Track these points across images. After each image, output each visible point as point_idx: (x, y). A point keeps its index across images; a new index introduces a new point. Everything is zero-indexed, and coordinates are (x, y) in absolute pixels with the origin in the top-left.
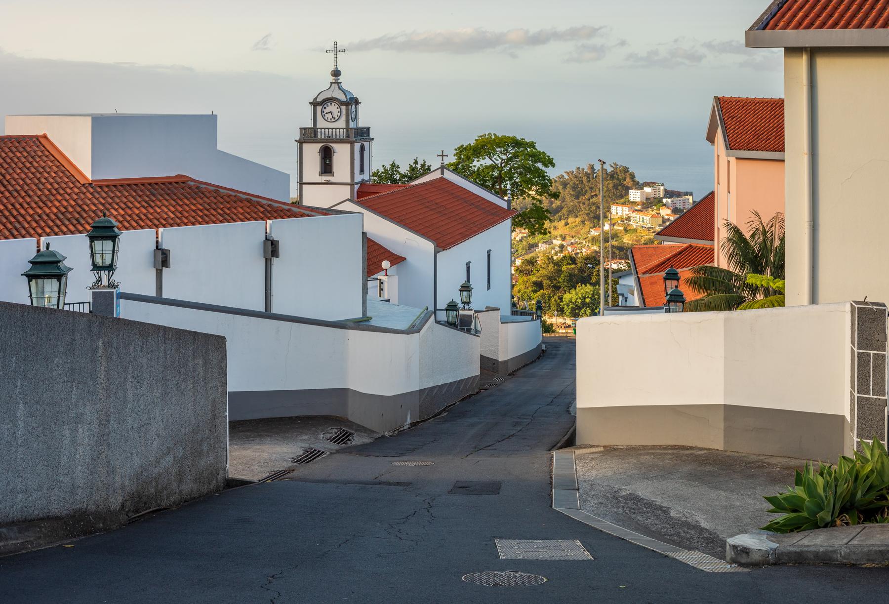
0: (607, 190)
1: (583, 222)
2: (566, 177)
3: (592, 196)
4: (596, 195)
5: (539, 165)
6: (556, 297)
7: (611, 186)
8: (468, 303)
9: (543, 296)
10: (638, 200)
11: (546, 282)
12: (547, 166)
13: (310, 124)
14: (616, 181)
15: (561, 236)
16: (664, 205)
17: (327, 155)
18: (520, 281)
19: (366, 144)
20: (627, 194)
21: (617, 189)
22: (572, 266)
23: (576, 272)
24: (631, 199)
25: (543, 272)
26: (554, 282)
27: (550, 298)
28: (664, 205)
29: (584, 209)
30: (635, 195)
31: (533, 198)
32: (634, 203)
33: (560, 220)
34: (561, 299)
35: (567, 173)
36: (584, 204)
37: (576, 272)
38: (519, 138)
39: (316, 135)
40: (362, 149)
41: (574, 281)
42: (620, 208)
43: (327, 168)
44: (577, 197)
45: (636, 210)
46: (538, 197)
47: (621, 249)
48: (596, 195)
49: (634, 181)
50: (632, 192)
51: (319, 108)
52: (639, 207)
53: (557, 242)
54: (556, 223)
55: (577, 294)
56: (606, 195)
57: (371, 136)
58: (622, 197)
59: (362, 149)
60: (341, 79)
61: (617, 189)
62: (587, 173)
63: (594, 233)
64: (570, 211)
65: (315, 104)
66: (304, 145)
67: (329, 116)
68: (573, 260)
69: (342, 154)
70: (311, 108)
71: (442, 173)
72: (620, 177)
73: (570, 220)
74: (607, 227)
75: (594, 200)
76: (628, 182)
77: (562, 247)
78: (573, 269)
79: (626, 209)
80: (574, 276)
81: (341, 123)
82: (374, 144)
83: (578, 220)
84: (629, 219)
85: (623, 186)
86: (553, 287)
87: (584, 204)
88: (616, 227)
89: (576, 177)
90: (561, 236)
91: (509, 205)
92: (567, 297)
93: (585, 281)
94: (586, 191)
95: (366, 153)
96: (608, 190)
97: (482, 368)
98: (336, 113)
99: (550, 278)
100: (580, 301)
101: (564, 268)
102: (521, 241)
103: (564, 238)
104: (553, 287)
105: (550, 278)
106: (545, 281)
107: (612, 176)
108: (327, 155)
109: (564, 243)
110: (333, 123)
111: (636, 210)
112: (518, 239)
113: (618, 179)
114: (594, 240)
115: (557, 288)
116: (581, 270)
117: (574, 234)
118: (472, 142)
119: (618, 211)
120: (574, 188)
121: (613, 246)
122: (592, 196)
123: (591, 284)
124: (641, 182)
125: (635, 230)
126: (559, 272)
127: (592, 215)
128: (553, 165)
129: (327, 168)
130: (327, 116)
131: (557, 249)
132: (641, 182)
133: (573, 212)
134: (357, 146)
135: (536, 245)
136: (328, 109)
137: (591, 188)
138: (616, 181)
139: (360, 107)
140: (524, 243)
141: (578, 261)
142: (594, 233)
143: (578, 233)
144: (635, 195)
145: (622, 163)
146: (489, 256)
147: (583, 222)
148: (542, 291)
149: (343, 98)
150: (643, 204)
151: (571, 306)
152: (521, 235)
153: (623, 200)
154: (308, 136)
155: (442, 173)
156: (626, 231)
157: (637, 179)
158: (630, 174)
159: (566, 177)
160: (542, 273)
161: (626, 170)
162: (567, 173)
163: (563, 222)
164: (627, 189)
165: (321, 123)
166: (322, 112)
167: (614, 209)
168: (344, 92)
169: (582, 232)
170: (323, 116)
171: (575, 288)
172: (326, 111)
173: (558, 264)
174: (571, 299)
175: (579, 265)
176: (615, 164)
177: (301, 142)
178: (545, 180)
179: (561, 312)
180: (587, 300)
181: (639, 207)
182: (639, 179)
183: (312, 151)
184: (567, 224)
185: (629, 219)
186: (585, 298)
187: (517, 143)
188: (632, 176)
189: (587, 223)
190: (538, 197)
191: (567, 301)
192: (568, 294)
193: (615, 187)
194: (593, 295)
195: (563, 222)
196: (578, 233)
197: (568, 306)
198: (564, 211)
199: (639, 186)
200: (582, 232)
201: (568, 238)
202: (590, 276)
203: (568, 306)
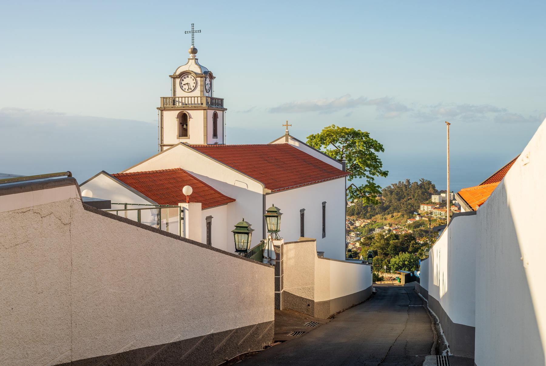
0: (418, 195)
1: (403, 215)
2: (392, 187)
3: (409, 199)
4: (411, 199)
5: (372, 150)
6: (386, 260)
7: (420, 193)
8: (276, 231)
9: (377, 260)
10: (437, 201)
11: (379, 251)
12: (378, 151)
13: (170, 94)
14: (423, 190)
15: (389, 224)
16: (453, 205)
17: (184, 120)
18: (363, 250)
19: (219, 113)
20: (430, 198)
21: (424, 195)
22: (396, 241)
23: (399, 245)
24: (433, 201)
25: (378, 244)
26: (385, 251)
27: (382, 261)
28: (453, 205)
29: (404, 208)
30: (435, 198)
31: (368, 177)
32: (435, 203)
33: (389, 214)
34: (389, 262)
35: (393, 185)
36: (403, 204)
37: (399, 245)
38: (356, 130)
39: (174, 102)
40: (215, 116)
41: (397, 250)
42: (426, 207)
43: (184, 132)
44: (399, 200)
45: (436, 208)
46: (371, 176)
47: (426, 232)
48: (411, 199)
49: (434, 190)
50: (433, 197)
51: (178, 81)
52: (438, 206)
53: (387, 228)
54: (386, 216)
55: (399, 258)
56: (417, 198)
57: (225, 107)
58: (427, 200)
59: (215, 116)
60: (198, 56)
61: (424, 195)
62: (405, 185)
63: (410, 222)
64: (395, 209)
65: (174, 77)
66: (164, 112)
67: (186, 87)
68: (397, 237)
69: (198, 121)
70: (171, 80)
71: (287, 140)
72: (426, 187)
73: (395, 214)
74: (418, 218)
75: (409, 201)
76: (431, 190)
77: (390, 231)
78: (397, 243)
79: (430, 207)
80: (398, 247)
81: (197, 93)
82: (227, 113)
83: (400, 214)
84: (431, 213)
85: (428, 193)
86: (384, 254)
87: (403, 204)
88: (423, 218)
89: (398, 187)
90: (389, 224)
91: (344, 167)
92: (393, 260)
93: (404, 250)
94: (405, 196)
95: (219, 121)
96: (418, 195)
97: (278, 313)
98: (192, 84)
99: (382, 249)
100: (401, 263)
101: (391, 242)
102: (364, 227)
103: (391, 225)
104: (384, 254)
105: (382, 249)
106: (378, 251)
107: (421, 187)
108: (184, 120)
109: (391, 228)
110: (191, 93)
111: (436, 208)
112: (362, 226)
113: (424, 189)
114: (409, 226)
115: (386, 255)
116: (402, 244)
117: (397, 223)
118: (320, 133)
119: (424, 208)
120: (397, 194)
121: (421, 230)
122: (409, 199)
123: (409, 252)
124: (439, 190)
125: (436, 220)
126: (388, 244)
127: (408, 211)
128: (383, 151)
129: (184, 132)
130: (184, 87)
131: (387, 232)
132: (439, 190)
133: (396, 209)
134: (211, 113)
135: (374, 230)
136: (186, 81)
137: (408, 194)
138: (423, 190)
139: (214, 82)
140: (366, 228)
141: (400, 237)
142: (410, 222)
143: (400, 222)
144: (435, 198)
145: (427, 178)
146: (324, 207)
147: (403, 215)
148: (377, 257)
149: (198, 71)
150: (440, 204)
151: (396, 266)
152: (364, 224)
153: (427, 202)
154: (168, 104)
155: (287, 140)
156: (430, 220)
157: (436, 188)
158: (432, 185)
159: (392, 187)
160: (376, 245)
161: (430, 183)
162: (393, 185)
163: (390, 215)
164: (430, 195)
165: (179, 93)
166: (181, 83)
167: (422, 207)
168: (200, 67)
169: (402, 221)
170: (181, 87)
171: (398, 255)
172: (183, 83)
173: (387, 239)
174: (396, 262)
175: (401, 240)
176: (423, 179)
177: (162, 110)
178: (376, 162)
179: (389, 270)
180: (406, 263)
181: (438, 206)
182: (438, 188)
183: (171, 119)
184: (392, 217)
185: (431, 213)
186: (405, 261)
187: (356, 134)
188: (434, 187)
189: (405, 216)
190: (371, 176)
191: (393, 263)
192: (393, 259)
193: (423, 193)
194: (410, 259)
195: (390, 215)
196: (400, 222)
197: (394, 266)
198: (391, 208)
199: (438, 193)
200: (402, 221)
201: (393, 225)
202: (407, 248)
203: (394, 266)
